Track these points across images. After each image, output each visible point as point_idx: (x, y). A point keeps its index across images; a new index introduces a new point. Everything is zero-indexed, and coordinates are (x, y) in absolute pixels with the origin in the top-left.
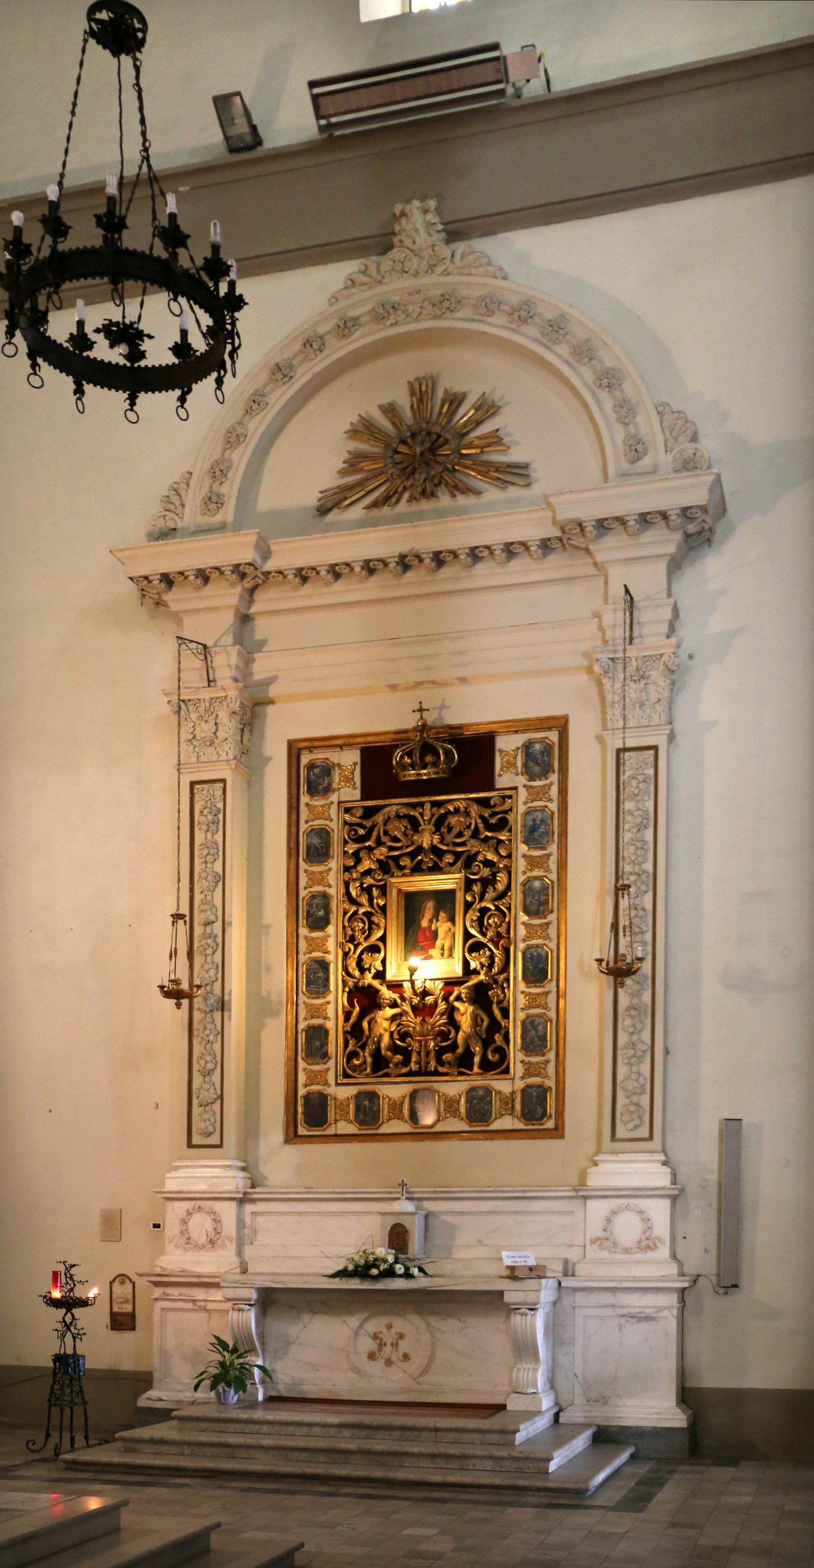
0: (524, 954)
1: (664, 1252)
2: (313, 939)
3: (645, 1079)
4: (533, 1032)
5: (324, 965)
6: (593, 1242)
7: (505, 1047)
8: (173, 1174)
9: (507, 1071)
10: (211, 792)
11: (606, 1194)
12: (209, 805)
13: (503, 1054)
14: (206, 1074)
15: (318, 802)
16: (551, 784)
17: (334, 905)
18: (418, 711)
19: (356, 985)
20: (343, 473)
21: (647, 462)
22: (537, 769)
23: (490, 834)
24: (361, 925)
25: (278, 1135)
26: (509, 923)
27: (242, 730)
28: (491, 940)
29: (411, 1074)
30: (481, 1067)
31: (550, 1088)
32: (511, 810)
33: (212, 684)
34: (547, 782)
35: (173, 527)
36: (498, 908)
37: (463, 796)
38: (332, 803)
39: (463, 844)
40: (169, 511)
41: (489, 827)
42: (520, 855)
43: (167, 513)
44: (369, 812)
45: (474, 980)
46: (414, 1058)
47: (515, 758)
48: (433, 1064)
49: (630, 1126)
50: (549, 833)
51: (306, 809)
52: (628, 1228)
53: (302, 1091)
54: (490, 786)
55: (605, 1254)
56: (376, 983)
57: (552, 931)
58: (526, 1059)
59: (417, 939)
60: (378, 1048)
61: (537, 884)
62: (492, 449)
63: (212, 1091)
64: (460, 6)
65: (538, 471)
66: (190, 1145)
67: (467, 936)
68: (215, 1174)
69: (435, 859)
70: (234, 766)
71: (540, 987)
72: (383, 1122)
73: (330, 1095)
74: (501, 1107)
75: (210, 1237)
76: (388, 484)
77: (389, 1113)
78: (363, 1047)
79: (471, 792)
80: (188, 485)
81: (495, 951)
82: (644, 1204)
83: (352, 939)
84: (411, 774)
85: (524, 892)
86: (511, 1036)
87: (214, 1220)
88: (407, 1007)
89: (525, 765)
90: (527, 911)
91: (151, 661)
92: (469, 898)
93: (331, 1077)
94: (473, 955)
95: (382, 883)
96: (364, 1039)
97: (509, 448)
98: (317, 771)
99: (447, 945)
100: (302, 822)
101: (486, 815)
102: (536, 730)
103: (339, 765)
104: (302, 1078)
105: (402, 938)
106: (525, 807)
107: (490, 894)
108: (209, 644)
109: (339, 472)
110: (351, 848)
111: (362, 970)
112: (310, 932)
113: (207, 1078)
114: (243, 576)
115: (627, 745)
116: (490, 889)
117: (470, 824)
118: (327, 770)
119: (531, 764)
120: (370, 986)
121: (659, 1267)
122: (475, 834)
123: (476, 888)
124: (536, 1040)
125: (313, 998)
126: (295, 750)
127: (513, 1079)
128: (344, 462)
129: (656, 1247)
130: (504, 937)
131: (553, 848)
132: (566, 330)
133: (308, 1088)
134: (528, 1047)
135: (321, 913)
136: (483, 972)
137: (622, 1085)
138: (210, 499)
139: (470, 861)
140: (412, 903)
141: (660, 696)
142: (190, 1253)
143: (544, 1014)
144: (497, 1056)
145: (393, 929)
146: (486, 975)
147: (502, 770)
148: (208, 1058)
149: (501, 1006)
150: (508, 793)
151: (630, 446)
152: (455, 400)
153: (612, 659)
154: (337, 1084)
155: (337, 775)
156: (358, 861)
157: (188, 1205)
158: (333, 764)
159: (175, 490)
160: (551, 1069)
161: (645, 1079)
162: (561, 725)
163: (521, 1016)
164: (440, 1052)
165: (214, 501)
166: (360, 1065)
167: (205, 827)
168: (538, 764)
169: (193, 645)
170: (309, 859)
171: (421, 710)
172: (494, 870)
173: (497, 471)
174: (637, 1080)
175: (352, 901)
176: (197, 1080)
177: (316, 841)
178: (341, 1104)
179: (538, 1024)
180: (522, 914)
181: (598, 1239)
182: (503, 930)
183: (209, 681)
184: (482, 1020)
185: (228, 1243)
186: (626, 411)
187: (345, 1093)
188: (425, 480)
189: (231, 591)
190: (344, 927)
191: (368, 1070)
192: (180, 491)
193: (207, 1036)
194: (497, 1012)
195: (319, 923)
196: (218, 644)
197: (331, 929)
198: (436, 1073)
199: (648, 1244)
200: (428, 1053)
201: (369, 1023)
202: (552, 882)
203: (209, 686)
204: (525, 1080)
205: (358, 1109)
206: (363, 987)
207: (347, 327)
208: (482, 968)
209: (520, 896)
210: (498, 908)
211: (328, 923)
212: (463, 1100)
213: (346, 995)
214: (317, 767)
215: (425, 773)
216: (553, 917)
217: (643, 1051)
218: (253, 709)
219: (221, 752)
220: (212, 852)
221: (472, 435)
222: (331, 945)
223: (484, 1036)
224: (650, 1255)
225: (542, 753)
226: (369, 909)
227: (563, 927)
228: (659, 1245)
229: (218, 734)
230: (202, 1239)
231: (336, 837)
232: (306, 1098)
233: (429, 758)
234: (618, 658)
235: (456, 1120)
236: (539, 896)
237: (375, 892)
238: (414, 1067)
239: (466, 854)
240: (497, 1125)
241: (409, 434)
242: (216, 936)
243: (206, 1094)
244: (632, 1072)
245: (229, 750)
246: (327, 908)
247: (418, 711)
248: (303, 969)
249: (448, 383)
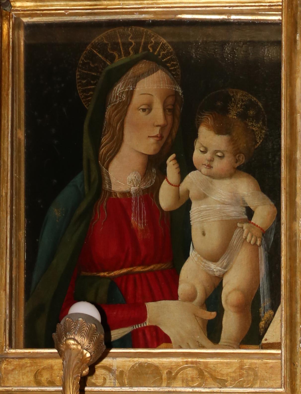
99: (235, 283)
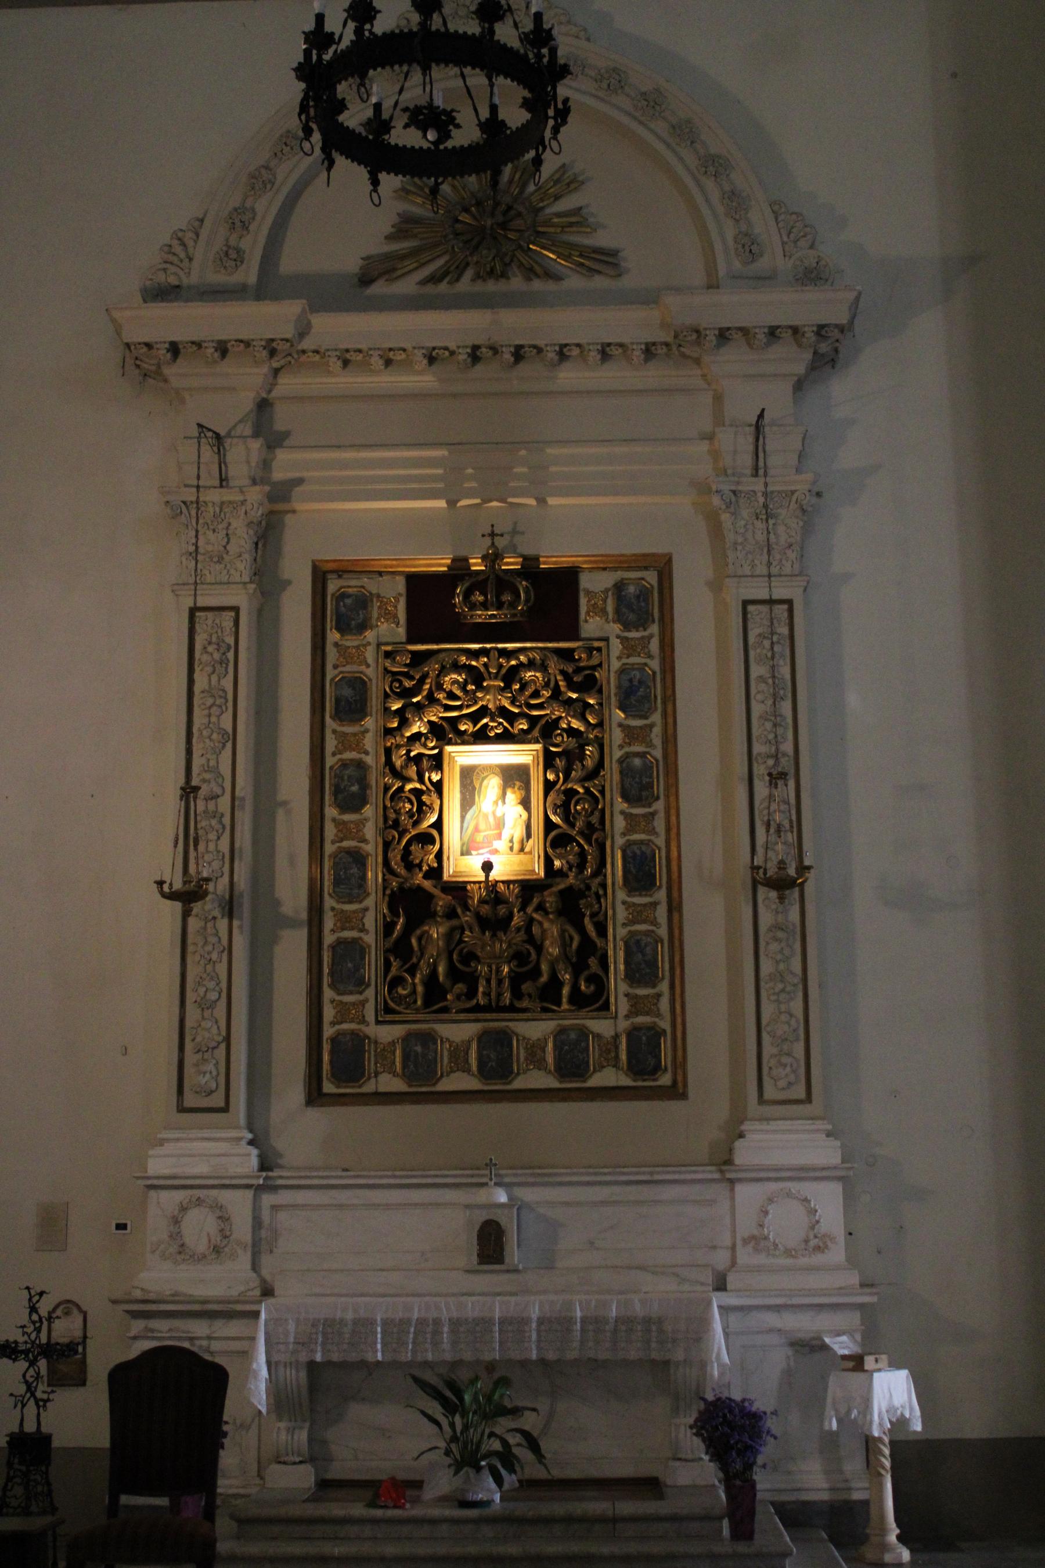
0: (624, 852)
1: (837, 1254)
2: (344, 823)
3: (797, 1021)
4: (640, 956)
6: (746, 1241)
8: (159, 1151)
9: (606, 1007)
10: (218, 621)
11: (761, 1175)
12: (214, 639)
13: (600, 984)
14: (207, 1005)
15: (351, 641)
16: (651, 636)
17: (372, 779)
18: (493, 532)
19: (401, 888)
22: (632, 617)
23: (575, 696)
24: (408, 806)
25: (297, 1094)
26: (603, 811)
27: (257, 544)
28: (581, 833)
29: (478, 1009)
30: (571, 1001)
32: (600, 665)
33: (224, 483)
34: (646, 634)
35: (177, 283)
36: (587, 791)
37: (540, 645)
38: (369, 644)
39: (540, 707)
40: (171, 263)
41: (572, 686)
42: (614, 725)
43: (168, 266)
47: (605, 601)
48: (507, 998)
49: (782, 1084)
51: (335, 650)
53: (328, 1032)
54: (573, 634)
55: (762, 1259)
56: (427, 884)
57: (659, 824)
58: (631, 991)
60: (434, 973)
61: (637, 762)
62: (574, 229)
63: (215, 1030)
66: (182, 1109)
68: (219, 1151)
69: (505, 724)
70: (251, 591)
71: (646, 895)
72: (442, 1076)
73: (369, 1038)
74: (600, 1055)
75: (213, 1241)
76: (446, 258)
77: (450, 1062)
78: (412, 971)
79: (550, 641)
80: (198, 235)
81: (586, 847)
84: (481, 616)
85: (621, 772)
86: (611, 960)
87: (220, 1218)
88: (467, 918)
89: (617, 611)
90: (625, 797)
91: (146, 450)
92: (551, 777)
94: (558, 851)
95: (436, 751)
96: (415, 960)
97: (595, 230)
98: (348, 601)
100: (329, 667)
101: (570, 670)
102: (629, 569)
103: (378, 596)
104: (329, 1013)
106: (620, 664)
108: (223, 433)
109: (386, 238)
112: (340, 814)
113: (207, 1013)
114: (273, 353)
115: (774, 597)
116: (577, 765)
117: (549, 680)
118: (363, 602)
119: (624, 610)
120: (420, 888)
122: (556, 694)
124: (643, 966)
125: (343, 903)
126: (320, 576)
127: (616, 1017)
128: (393, 226)
129: (826, 1247)
130: (597, 829)
131: (656, 718)
132: (663, 107)
133: (337, 1027)
134: (633, 976)
135: (355, 788)
136: (572, 875)
137: (769, 1029)
138: (227, 254)
141: (792, 540)
142: (183, 1267)
143: (653, 931)
144: (592, 988)
146: (576, 877)
147: (588, 613)
148: (211, 985)
149: (595, 919)
150: (596, 644)
151: (743, 246)
153: (734, 492)
154: (378, 1022)
155: (375, 609)
156: (404, 723)
157: (180, 1196)
158: (371, 594)
159: (179, 239)
160: (664, 1004)
161: (797, 1021)
162: (664, 566)
163: (622, 932)
164: (516, 980)
165: (232, 256)
166: (406, 996)
167: (209, 669)
168: (633, 611)
169: (210, 434)
170: (337, 716)
171: (493, 535)
172: (581, 741)
173: (581, 256)
174: (788, 1023)
176: (193, 1014)
177: (347, 692)
178: (533, 1046)
179: (646, 945)
180: (620, 800)
181: (753, 1237)
182: (595, 819)
183: (221, 480)
184: (571, 938)
185: (240, 1251)
186: (736, 202)
187: (388, 1033)
188: (494, 258)
189: (256, 370)
190: (385, 807)
191: (419, 1003)
192: (186, 240)
193: (209, 953)
195: (352, 802)
196: (233, 433)
197: (368, 810)
198: (512, 1009)
200: (500, 982)
201: (420, 939)
202: (657, 761)
203: (221, 486)
204: (632, 1020)
205: (406, 1057)
206: (410, 889)
208: (570, 869)
209: (616, 777)
210: (587, 791)
211: (363, 801)
212: (550, 1045)
213: (387, 898)
214: (349, 596)
216: (659, 806)
217: (795, 985)
219: (232, 571)
220: (218, 702)
221: (548, 211)
223: (574, 960)
224: (819, 1259)
225: (638, 597)
226: (418, 786)
227: (673, 819)
228: (829, 1243)
229: (228, 547)
230: (202, 1247)
231: (374, 689)
232: (333, 1040)
233: (507, 597)
234: (740, 492)
235: (542, 1073)
236: (641, 777)
238: (481, 1000)
239: (543, 722)
240: (596, 1080)
241: (474, 202)
242: (222, 815)
243: (207, 1035)
244: (780, 1013)
245: (242, 568)
246: (363, 783)
247: (493, 532)
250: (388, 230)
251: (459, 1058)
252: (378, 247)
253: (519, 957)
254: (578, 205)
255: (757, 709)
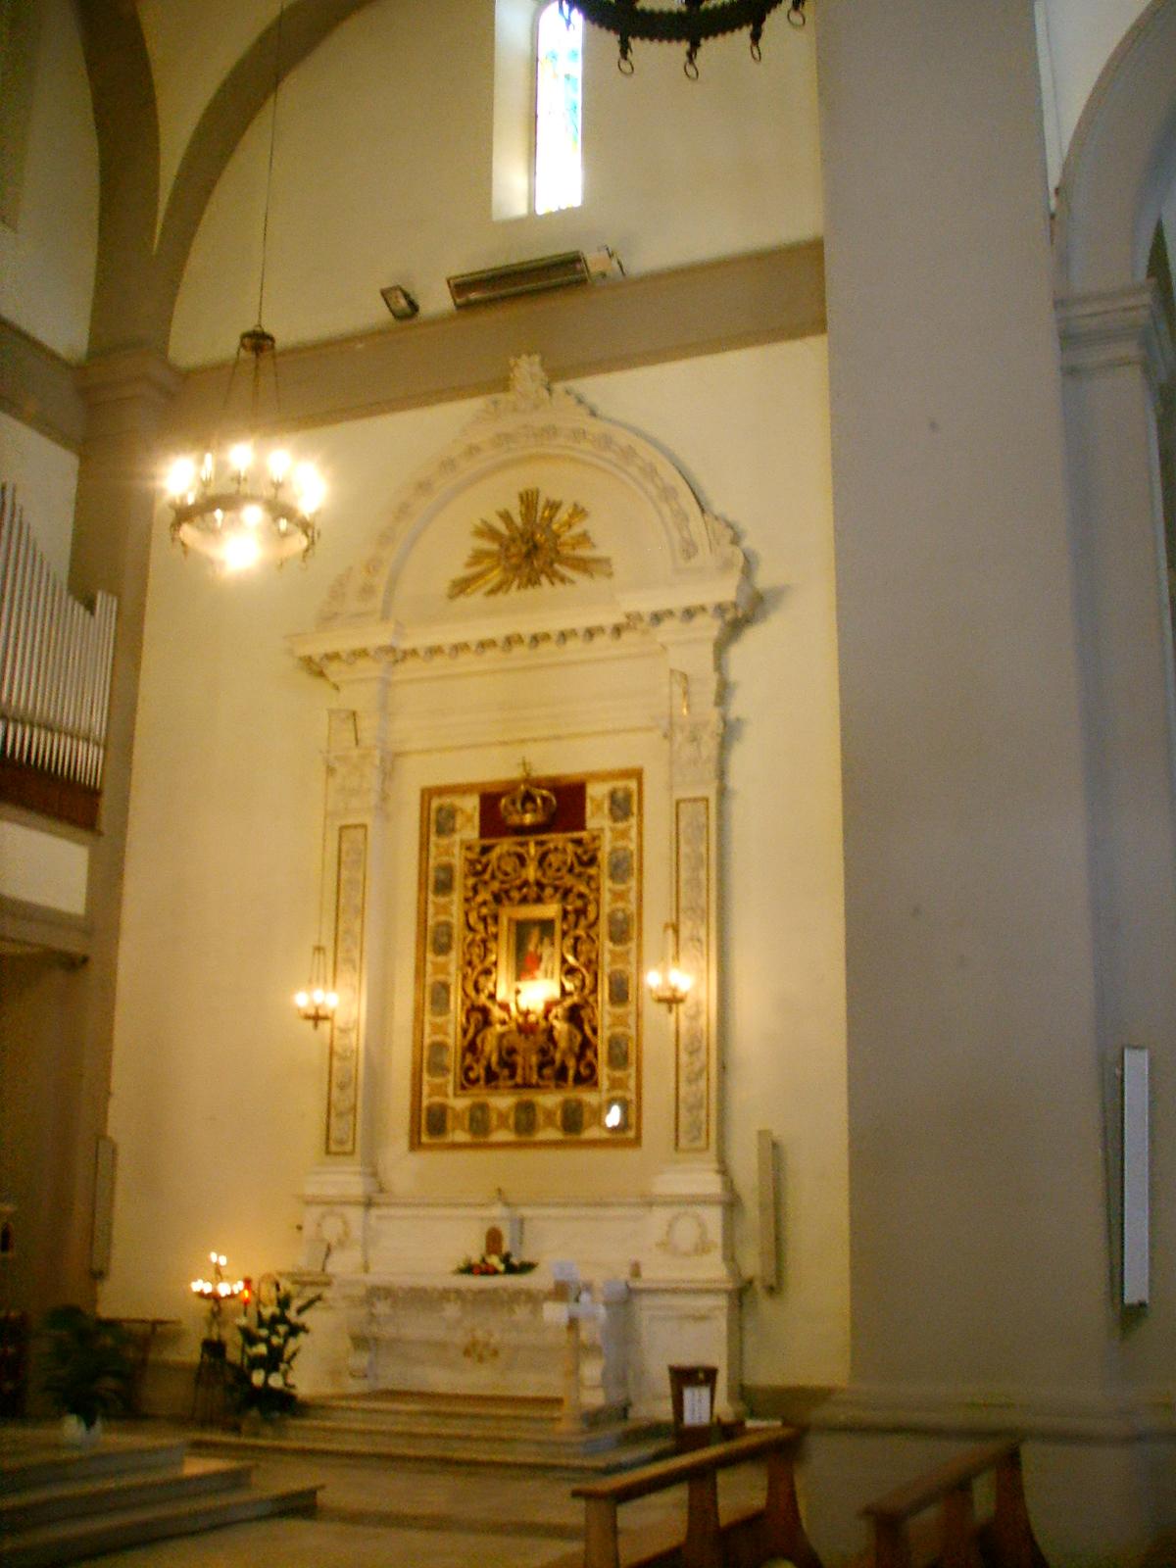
5: (445, 987)
7: (594, 1061)
11: (670, 1201)
13: (592, 1068)
15: (444, 841)
20: (469, 565)
21: (695, 562)
25: (404, 1142)
29: (517, 1086)
31: (631, 1100)
41: (582, 863)
44: (485, 850)
45: (568, 1002)
46: (519, 1071)
48: (534, 1078)
50: (628, 872)
52: (686, 1233)
53: (425, 1103)
54: (581, 826)
56: (489, 1004)
57: (633, 958)
59: (525, 966)
61: (620, 915)
64: (732, 3)
65: (617, 566)
67: (564, 961)
68: (348, 1180)
78: (478, 1061)
82: (699, 1210)
83: (470, 963)
89: (611, 810)
93: (450, 1089)
105: (513, 963)
107: (583, 922)
110: (471, 881)
111: (477, 990)
121: (713, 1269)
123: (572, 918)
139: (567, 893)
140: (522, 929)
145: (502, 955)
152: (554, 507)
160: (632, 1083)
162: (637, 774)
164: (541, 1066)
175: (471, 928)
182: (593, 956)
184: (575, 1037)
187: (460, 1103)
194: (587, 1028)
195: (443, 949)
198: (537, 1086)
199: (702, 1248)
205: (472, 1119)
207: (473, 450)
210: (588, 936)
215: (528, 819)
218: (390, 764)
222: (453, 968)
232: (430, 1109)
237: (490, 921)
248: (428, 990)
249: (548, 493)
250: (466, 559)
251: (502, 1117)
252: (461, 572)
253: (543, 1052)
254: (498, 518)
255: (684, 875)
